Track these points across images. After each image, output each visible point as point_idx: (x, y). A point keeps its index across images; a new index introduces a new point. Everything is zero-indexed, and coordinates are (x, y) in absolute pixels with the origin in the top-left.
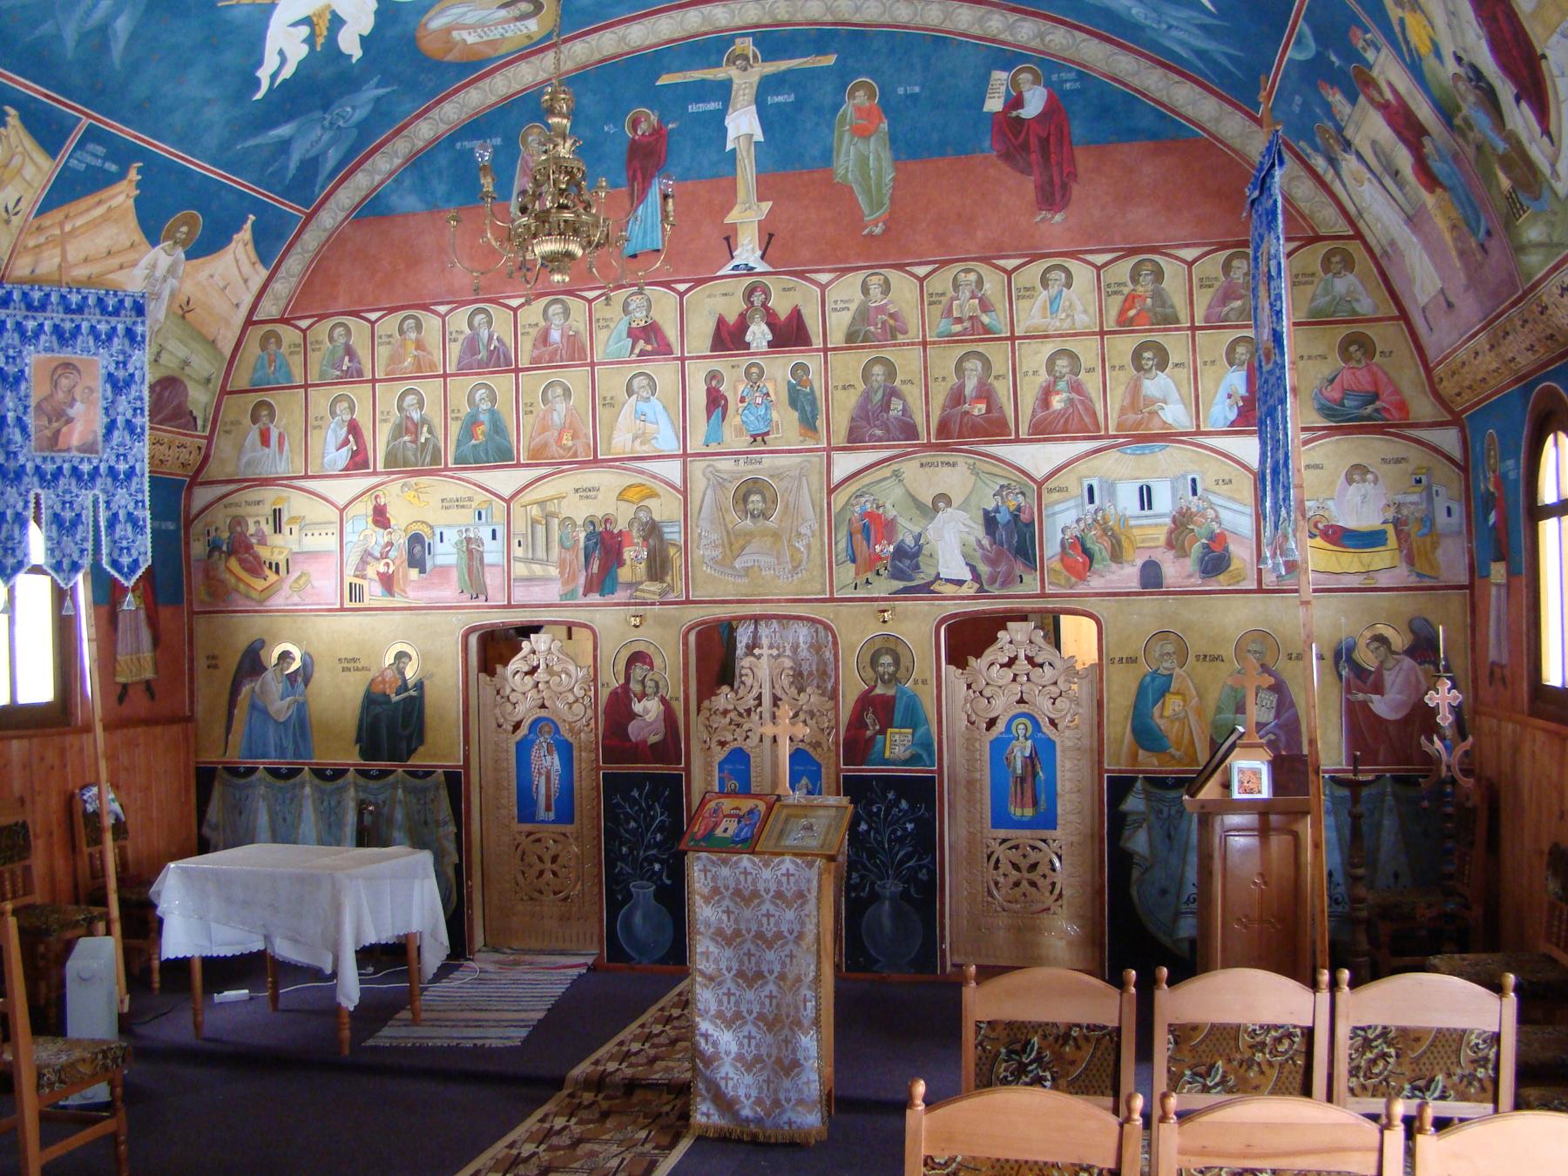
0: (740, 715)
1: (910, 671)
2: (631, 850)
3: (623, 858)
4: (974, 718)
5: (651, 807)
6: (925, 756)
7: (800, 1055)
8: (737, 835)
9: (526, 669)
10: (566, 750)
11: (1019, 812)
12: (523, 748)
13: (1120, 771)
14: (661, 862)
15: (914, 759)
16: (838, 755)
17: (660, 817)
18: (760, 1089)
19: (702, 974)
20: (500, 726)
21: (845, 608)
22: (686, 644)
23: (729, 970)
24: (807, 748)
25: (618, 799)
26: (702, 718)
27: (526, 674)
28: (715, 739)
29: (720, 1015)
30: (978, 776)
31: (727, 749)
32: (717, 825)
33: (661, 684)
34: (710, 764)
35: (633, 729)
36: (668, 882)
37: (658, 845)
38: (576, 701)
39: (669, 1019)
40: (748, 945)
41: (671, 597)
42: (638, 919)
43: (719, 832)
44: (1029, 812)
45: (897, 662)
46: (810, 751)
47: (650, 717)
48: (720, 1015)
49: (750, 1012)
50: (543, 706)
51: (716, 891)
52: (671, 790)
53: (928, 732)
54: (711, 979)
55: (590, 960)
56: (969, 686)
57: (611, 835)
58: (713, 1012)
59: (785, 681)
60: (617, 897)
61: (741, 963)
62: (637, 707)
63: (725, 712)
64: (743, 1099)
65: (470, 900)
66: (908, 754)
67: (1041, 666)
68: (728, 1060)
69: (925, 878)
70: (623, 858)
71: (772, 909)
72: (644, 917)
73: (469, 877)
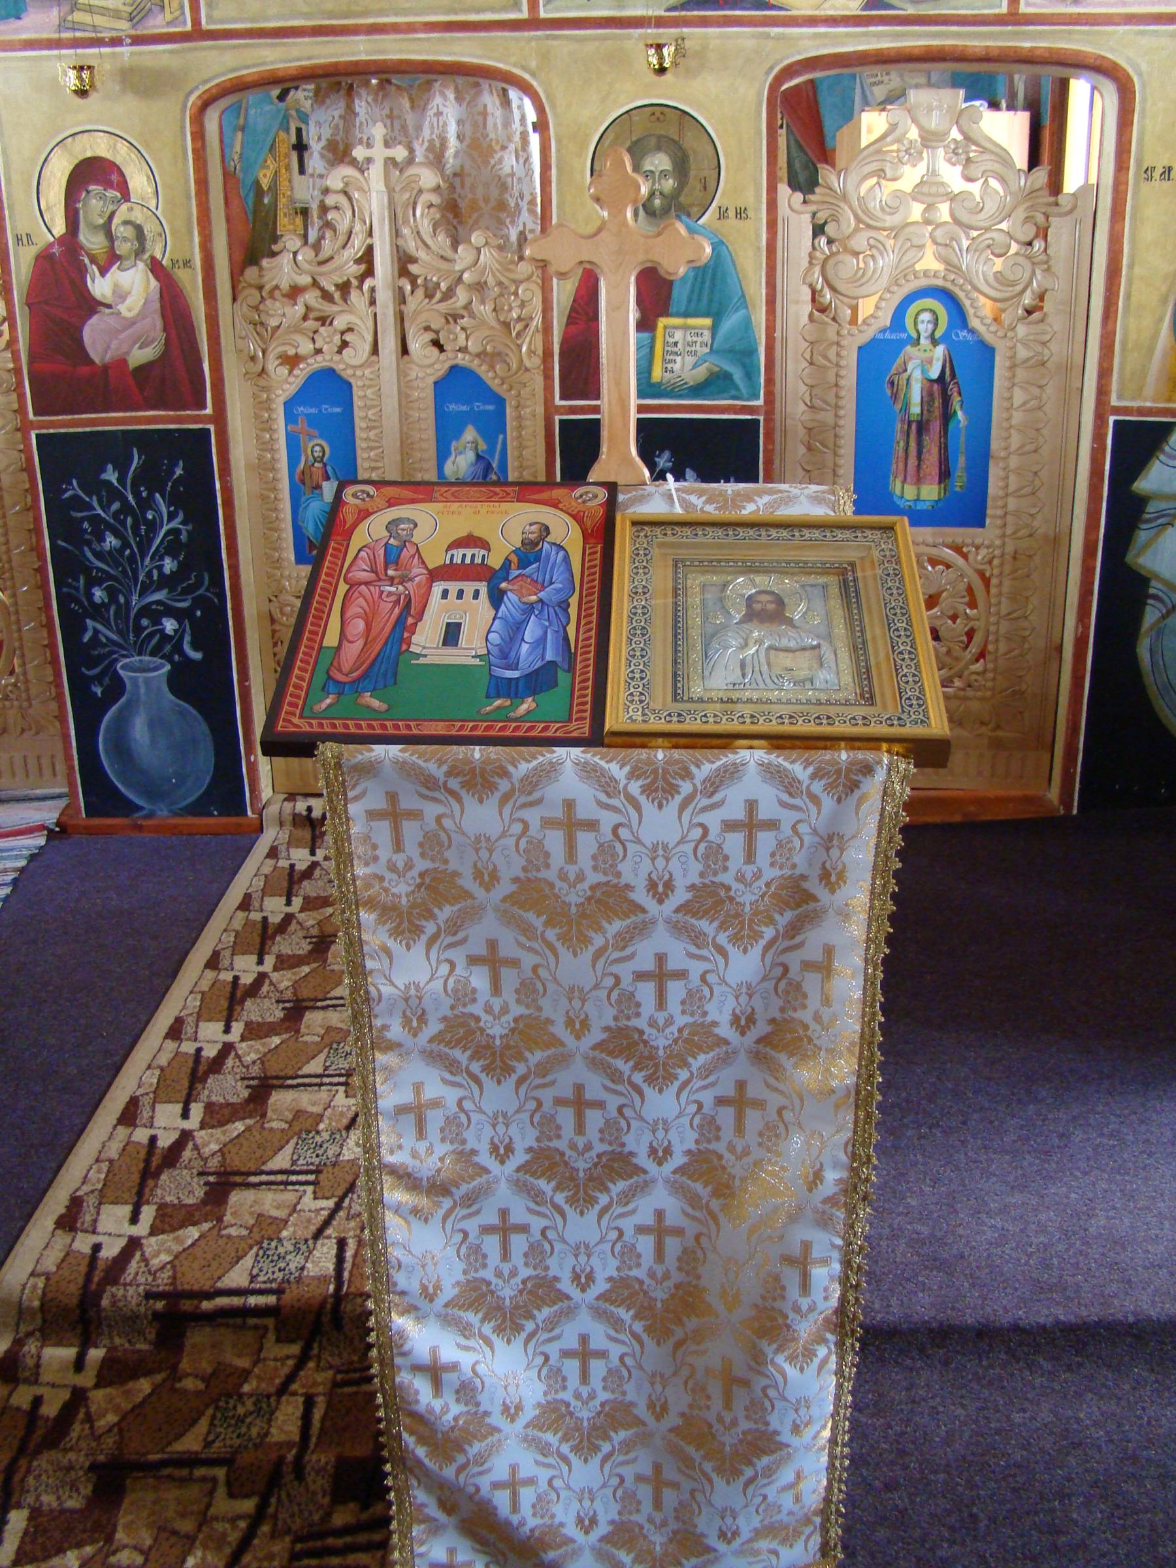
0: (327, 296)
1: (709, 189)
2: (112, 593)
3: (97, 611)
5: (146, 504)
6: (737, 375)
7: (779, 1421)
8: (506, 654)
11: (910, 492)
13: (1140, 411)
14: (171, 612)
15: (716, 383)
16: (548, 377)
17: (169, 521)
18: (629, 1500)
19: (406, 1178)
21: (564, 43)
22: (199, 135)
23: (502, 1151)
24: (475, 365)
25: (74, 489)
26: (243, 308)
28: (275, 349)
29: (476, 1295)
30: (828, 417)
31: (302, 372)
32: (409, 613)
33: (150, 228)
34: (267, 405)
35: (96, 337)
36: (197, 656)
37: (166, 581)
39: (236, 997)
40: (577, 1073)
41: (157, 24)
42: (139, 730)
43: (426, 638)
44: (930, 492)
45: (681, 167)
46: (482, 371)
47: (129, 308)
48: (476, 1295)
49: (584, 1280)
51: (437, 887)
52: (187, 469)
53: (747, 324)
54: (438, 1188)
55: (49, 814)
57: (68, 566)
58: (449, 1292)
59: (423, 218)
60: (93, 693)
61: (548, 1126)
62: (100, 287)
63: (295, 292)
64: (571, 1530)
66: (701, 373)
68: (512, 1430)
70: (97, 611)
71: (678, 954)
72: (151, 725)
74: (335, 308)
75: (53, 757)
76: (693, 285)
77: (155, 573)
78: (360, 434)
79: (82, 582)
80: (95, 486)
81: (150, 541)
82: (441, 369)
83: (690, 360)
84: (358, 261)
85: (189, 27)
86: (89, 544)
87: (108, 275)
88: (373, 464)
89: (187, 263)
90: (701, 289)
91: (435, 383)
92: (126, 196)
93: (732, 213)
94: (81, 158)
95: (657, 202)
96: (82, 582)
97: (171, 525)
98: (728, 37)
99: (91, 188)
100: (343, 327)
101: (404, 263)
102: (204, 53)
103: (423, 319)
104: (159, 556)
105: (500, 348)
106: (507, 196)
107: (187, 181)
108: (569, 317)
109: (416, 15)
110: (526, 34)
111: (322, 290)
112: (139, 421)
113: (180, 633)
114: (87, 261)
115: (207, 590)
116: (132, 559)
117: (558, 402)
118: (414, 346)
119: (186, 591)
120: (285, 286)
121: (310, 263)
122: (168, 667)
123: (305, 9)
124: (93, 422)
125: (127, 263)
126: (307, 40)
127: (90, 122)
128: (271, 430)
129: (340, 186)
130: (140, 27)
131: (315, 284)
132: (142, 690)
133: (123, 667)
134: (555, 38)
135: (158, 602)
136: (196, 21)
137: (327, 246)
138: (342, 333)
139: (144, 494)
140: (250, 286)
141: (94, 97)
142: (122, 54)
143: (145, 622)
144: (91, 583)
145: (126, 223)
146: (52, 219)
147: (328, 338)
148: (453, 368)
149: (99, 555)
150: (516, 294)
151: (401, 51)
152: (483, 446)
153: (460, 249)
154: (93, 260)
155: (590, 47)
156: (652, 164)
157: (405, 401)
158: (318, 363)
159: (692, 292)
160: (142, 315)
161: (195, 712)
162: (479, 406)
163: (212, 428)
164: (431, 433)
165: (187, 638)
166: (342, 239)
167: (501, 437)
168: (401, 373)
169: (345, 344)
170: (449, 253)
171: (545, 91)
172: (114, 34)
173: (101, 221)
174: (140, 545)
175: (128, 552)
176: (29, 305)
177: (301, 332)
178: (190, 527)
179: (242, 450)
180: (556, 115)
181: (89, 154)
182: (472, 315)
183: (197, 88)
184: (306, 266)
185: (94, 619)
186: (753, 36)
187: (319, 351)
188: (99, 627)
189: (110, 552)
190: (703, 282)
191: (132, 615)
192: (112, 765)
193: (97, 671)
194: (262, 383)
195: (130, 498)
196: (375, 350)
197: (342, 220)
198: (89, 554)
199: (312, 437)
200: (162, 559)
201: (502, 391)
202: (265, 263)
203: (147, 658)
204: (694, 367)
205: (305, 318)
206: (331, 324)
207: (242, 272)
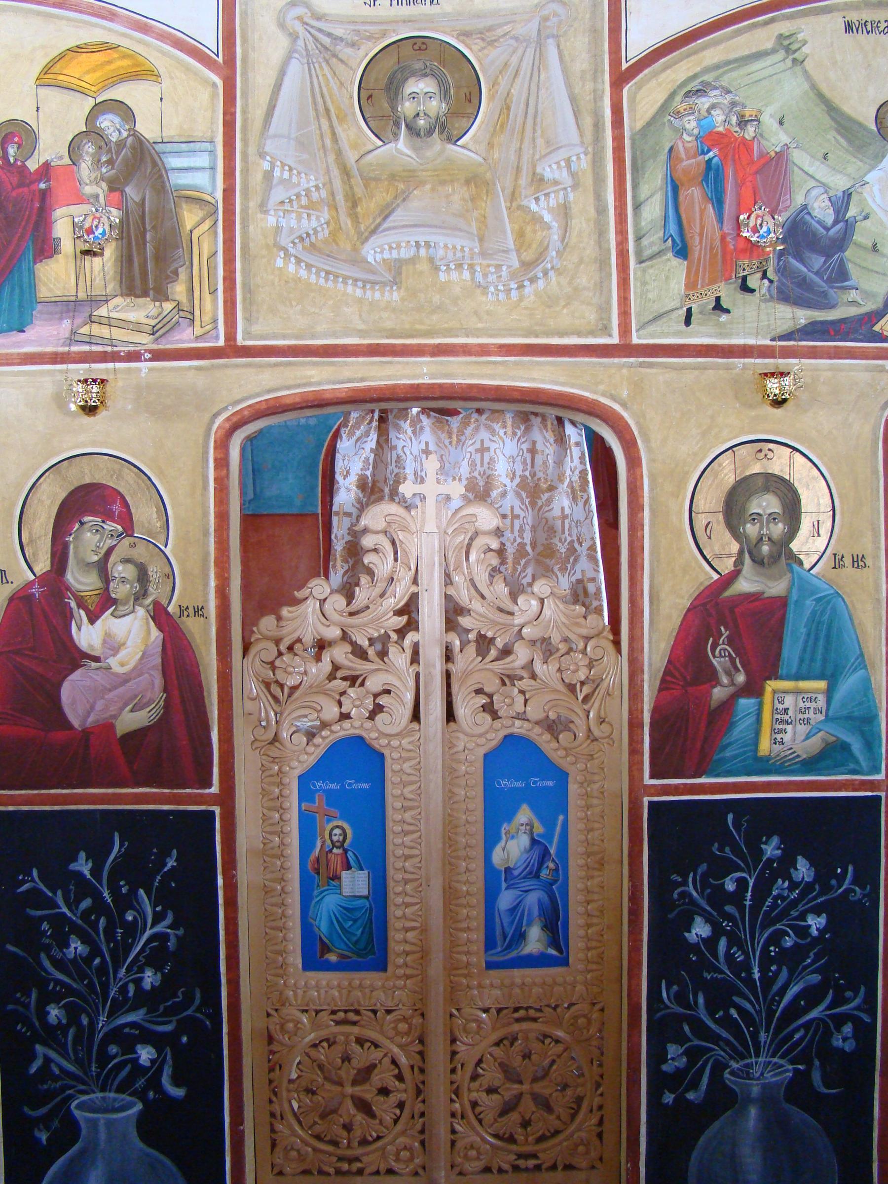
0: (360, 653)
2: (73, 1012)
3: (52, 1035)
5: (126, 902)
6: (856, 746)
14: (148, 1037)
15: (832, 755)
17: (151, 921)
31: (323, 742)
36: (179, 1092)
37: (145, 999)
41: (184, 339)
46: (543, 740)
53: (866, 686)
59: (478, 565)
62: (87, 635)
66: (815, 744)
69: (849, 1046)
70: (52, 1035)
74: (368, 666)
76: (806, 642)
77: (132, 988)
78: (392, 815)
79: (34, 996)
80: (60, 876)
82: (495, 739)
83: (802, 729)
84: (399, 613)
85: (221, 342)
86: (47, 949)
87: (99, 623)
88: (407, 852)
89: (199, 611)
90: (813, 652)
91: (485, 755)
92: (128, 528)
93: (848, 561)
94: (77, 484)
95: (765, 549)
96: (34, 996)
97: (158, 929)
98: (840, 369)
99: (87, 519)
100: (377, 688)
101: (453, 613)
102: (237, 371)
103: (473, 682)
104: (138, 967)
105: (564, 713)
106: (556, 541)
107: (206, 514)
108: (663, 681)
109: (491, 336)
110: (616, 360)
111: (353, 644)
112: (118, 799)
113: (157, 1065)
114: (73, 604)
115: (198, 1010)
116: (102, 970)
117: (648, 781)
118: (461, 711)
120: (308, 639)
121: (341, 613)
122: (139, 1106)
123: (362, 327)
124: (66, 800)
125: (122, 609)
126: (361, 359)
127: (94, 444)
128: (281, 809)
129: (381, 525)
130: (163, 340)
131: (345, 637)
132: (103, 1136)
133: (78, 1107)
134: (651, 365)
135: (133, 1025)
136: (231, 336)
137: (362, 595)
138: (376, 696)
140: (267, 638)
141: (102, 414)
142: (139, 370)
143: (113, 1049)
144: (46, 999)
146: (35, 555)
147: (357, 702)
148: (509, 739)
149: (59, 964)
150: (584, 652)
151: (472, 376)
152: (539, 829)
153: (520, 600)
154: (81, 605)
155: (689, 377)
156: (760, 506)
157: (450, 773)
158: (346, 729)
159: (804, 650)
160: (138, 671)
162: (536, 782)
163: (217, 810)
164: (478, 815)
165: (167, 1071)
166: (380, 587)
167: (561, 817)
168: (449, 744)
169: (378, 709)
170: (508, 605)
171: (638, 423)
172: (131, 348)
173: (96, 558)
174: (113, 953)
175: (97, 961)
177: (325, 693)
178: (181, 932)
179: (248, 832)
180: (649, 450)
181: (87, 480)
182: (534, 677)
183: (225, 409)
184: (335, 617)
185: (45, 1044)
186: (867, 369)
187: (345, 716)
188: (53, 1054)
189: (74, 961)
190: (817, 639)
193: (44, 1110)
194: (274, 752)
195: (106, 894)
196: (416, 716)
197: (382, 565)
198: (47, 964)
199: (330, 818)
200: (142, 971)
201: (564, 763)
202: (285, 611)
203: (112, 1095)
204: (807, 737)
205: (331, 677)
206: (362, 684)
207: (255, 623)
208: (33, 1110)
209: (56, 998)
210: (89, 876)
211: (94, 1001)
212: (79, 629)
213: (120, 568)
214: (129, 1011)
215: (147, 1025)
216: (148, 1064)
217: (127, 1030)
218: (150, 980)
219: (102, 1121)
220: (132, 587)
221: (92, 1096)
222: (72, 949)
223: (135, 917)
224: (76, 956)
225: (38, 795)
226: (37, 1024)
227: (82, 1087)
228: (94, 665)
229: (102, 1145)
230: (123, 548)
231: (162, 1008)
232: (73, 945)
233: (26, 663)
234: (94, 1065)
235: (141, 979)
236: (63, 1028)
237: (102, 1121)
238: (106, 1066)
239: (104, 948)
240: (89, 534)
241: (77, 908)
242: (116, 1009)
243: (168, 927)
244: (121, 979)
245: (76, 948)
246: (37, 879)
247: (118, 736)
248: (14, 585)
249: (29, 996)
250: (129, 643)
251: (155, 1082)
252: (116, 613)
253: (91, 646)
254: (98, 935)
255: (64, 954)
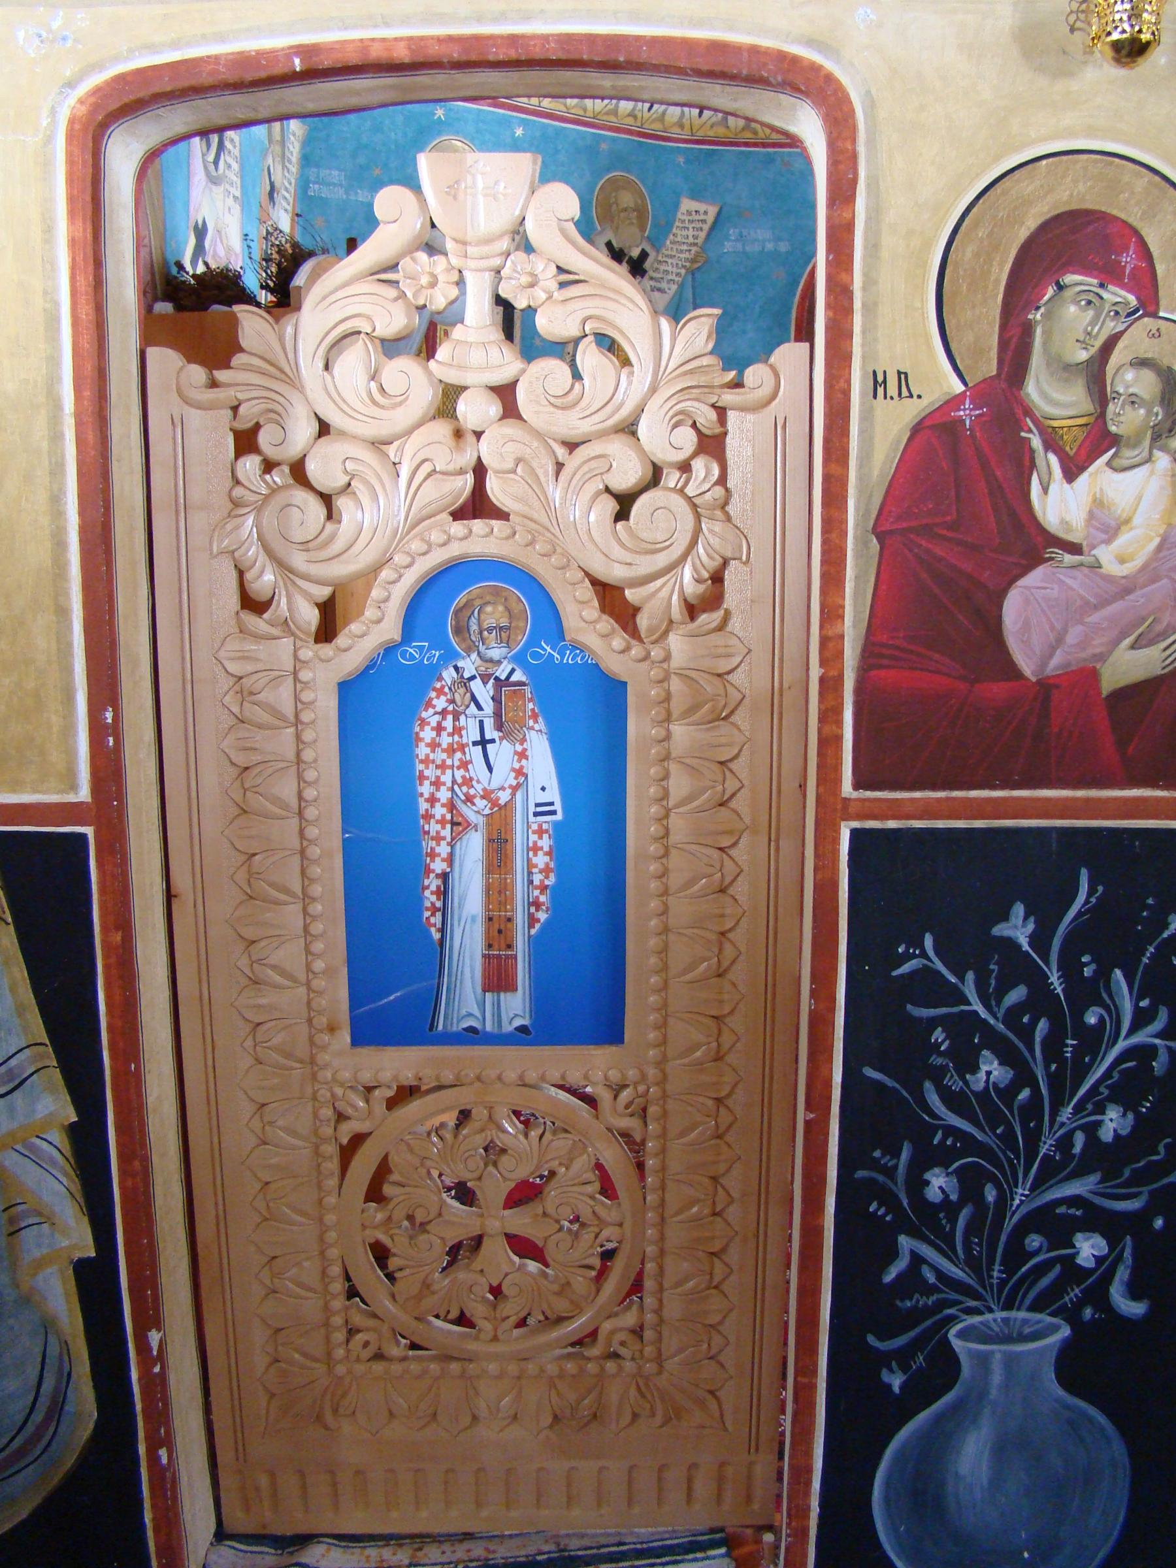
2: (971, 1182)
3: (930, 1220)
4: (265, 580)
5: (1087, 992)
9: (393, 320)
10: (592, 718)
12: (375, 706)
14: (1094, 1218)
20: (252, 604)
27: (391, 346)
35: (1036, 622)
36: (1134, 1309)
37: (1101, 1158)
38: (655, 476)
42: (972, 1457)
47: (1119, 557)
50: (477, 506)
56: (246, 442)
57: (873, 1122)
62: (1058, 503)
65: (160, 1413)
67: (564, 350)
70: (930, 1220)
72: (1001, 1450)
73: (149, 1316)
75: (693, 1466)
77: (1079, 1139)
79: (905, 1155)
80: (974, 948)
81: (1082, 1072)
87: (1083, 479)
96: (905, 1155)
97: (1139, 1038)
99: (1069, 278)
113: (1106, 1266)
114: (1036, 442)
116: (1032, 1110)
119: (1139, 1178)
122: (1065, 1331)
125: (1129, 455)
127: (1091, 131)
132: (997, 1377)
133: (961, 1335)
139: (1087, 972)
143: (1034, 1241)
144: (924, 1161)
145: (1142, 363)
149: (956, 1102)
154: (1051, 444)
161: (1101, 1419)
173: (1083, 356)
174: (1055, 1081)
175: (1025, 1094)
176: (880, 532)
191: (1009, 1224)
192: (893, 1528)
195: (1054, 979)
198: (933, 1099)
200: (1100, 1109)
203: (1022, 1314)
208: (881, 1339)
209: (942, 1158)
210: (1026, 947)
211: (1010, 1161)
212: (1045, 490)
213: (1129, 376)
214: (1067, 1179)
215: (1098, 1200)
216: (1091, 1264)
217: (1061, 1210)
218: (1112, 1125)
219: (998, 1356)
220: (1149, 412)
221: (988, 1316)
222: (982, 1075)
223: (1102, 1020)
224: (986, 1088)
225: (948, 799)
226: (905, 1203)
227: (973, 1303)
228: (1068, 558)
229: (994, 1393)
230: (1137, 339)
231: (1127, 1173)
232: (984, 1068)
233: (938, 551)
234: (997, 1267)
235: (1099, 1123)
236: (949, 1207)
237: (998, 1356)
238: (1014, 1268)
239: (1040, 1073)
240: (1073, 309)
241: (999, 1003)
242: (1049, 1173)
243: (1157, 1036)
244: (1063, 1124)
245: (989, 1073)
246: (931, 953)
247: (1105, 693)
248: (925, 402)
249: (897, 1155)
250: (1136, 521)
251: (1098, 1294)
252: (1117, 463)
253: (1064, 523)
254: (1032, 1051)
255: (966, 1083)
